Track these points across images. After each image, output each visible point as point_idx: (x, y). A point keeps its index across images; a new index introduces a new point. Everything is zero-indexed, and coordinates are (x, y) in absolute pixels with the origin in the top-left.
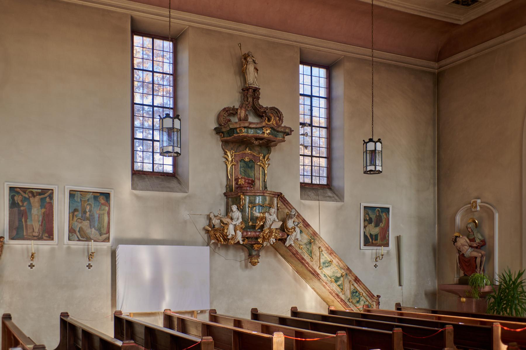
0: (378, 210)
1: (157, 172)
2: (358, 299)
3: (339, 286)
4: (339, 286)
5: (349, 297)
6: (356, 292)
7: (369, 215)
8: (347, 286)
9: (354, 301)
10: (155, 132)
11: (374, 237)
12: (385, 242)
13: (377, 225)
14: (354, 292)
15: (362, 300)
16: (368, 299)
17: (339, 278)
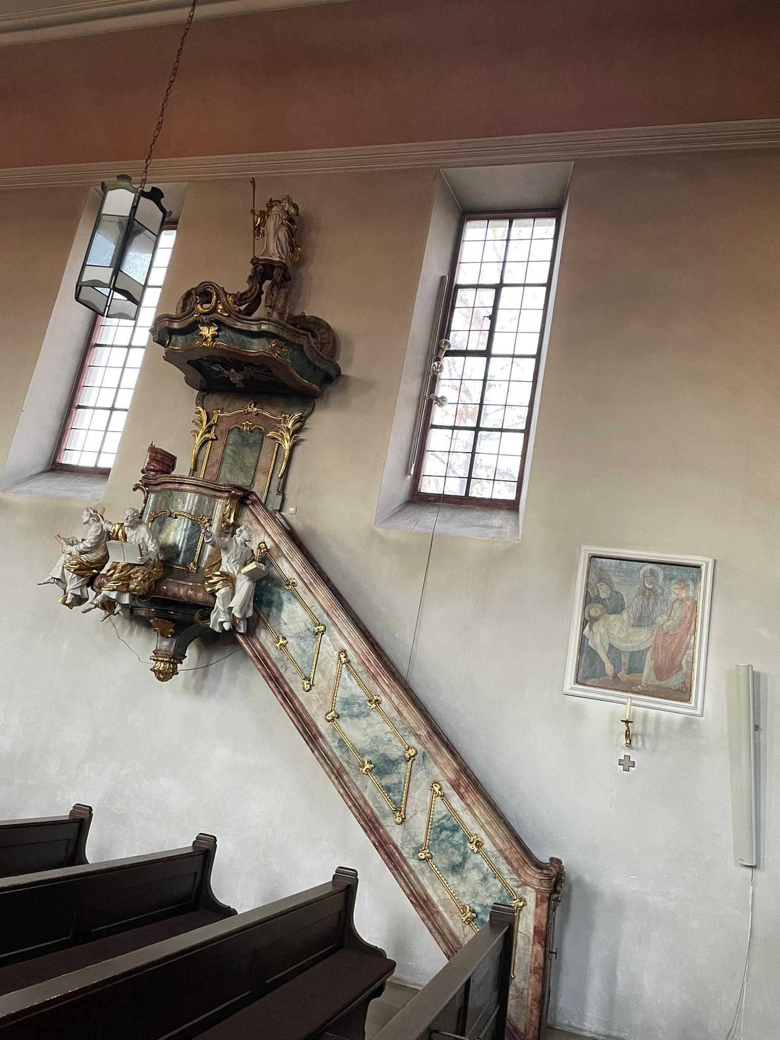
0: (652, 572)
1: (104, 198)
2: (458, 859)
3: (388, 789)
4: (388, 789)
5: (422, 839)
6: (455, 829)
7: (610, 584)
8: (419, 800)
9: (440, 861)
10: (98, 237)
11: (625, 659)
12: (674, 681)
13: (640, 621)
14: (443, 828)
15: (476, 866)
16: (504, 868)
17: (394, 763)
